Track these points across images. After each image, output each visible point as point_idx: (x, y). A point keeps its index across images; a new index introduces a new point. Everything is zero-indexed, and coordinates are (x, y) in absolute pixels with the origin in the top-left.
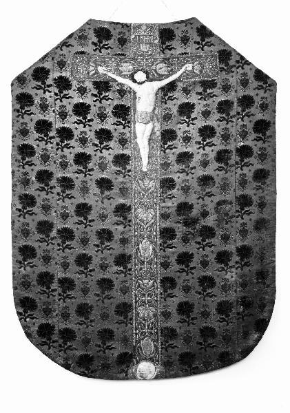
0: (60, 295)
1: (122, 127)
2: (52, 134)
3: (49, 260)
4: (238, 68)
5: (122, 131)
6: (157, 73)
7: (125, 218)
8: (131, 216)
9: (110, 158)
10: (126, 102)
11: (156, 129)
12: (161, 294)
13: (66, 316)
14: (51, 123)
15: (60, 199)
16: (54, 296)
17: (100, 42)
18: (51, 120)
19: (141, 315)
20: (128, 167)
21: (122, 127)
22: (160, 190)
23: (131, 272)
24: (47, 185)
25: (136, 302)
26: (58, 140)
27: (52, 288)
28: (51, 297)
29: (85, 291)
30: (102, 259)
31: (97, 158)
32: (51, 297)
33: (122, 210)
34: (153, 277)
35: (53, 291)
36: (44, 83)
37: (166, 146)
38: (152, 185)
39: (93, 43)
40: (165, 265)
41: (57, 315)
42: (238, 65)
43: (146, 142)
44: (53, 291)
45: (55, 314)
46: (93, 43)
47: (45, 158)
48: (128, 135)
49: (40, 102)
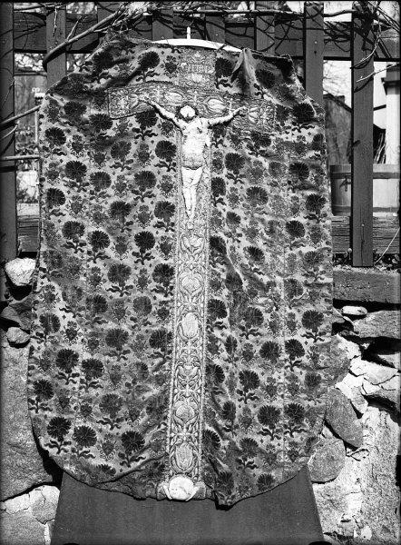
0: (82, 381)
1: (166, 169)
2: (77, 369)
3: (74, 336)
4: (293, 130)
5: (166, 173)
6: (208, 109)
7: (166, 284)
8: (175, 280)
9: (152, 208)
10: (173, 140)
11: (205, 176)
12: (206, 386)
13: (86, 411)
14: (85, 167)
15: (91, 259)
16: (75, 383)
17: (143, 128)
18: (86, 163)
19: (184, 283)
20: (172, 219)
21: (166, 169)
22: (208, 251)
23: (170, 356)
24: (79, 180)
25: (174, 395)
26: (90, 247)
27: (74, 372)
28: (71, 383)
29: (115, 379)
30: (141, 208)
31: (137, 272)
32: (71, 383)
33: (165, 272)
34: (197, 363)
35: (74, 375)
36: (61, 439)
37: (219, 80)
38: (201, 243)
39: (134, 254)
40: (213, 348)
41: (75, 408)
42: (293, 127)
43: (194, 191)
44: (74, 375)
45: (73, 406)
46: (134, 254)
47: (77, 208)
48: (173, 179)
49: (72, 141)
